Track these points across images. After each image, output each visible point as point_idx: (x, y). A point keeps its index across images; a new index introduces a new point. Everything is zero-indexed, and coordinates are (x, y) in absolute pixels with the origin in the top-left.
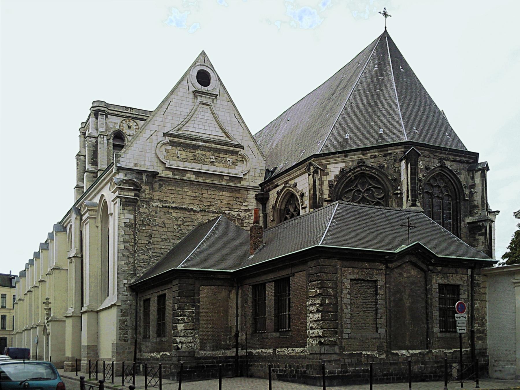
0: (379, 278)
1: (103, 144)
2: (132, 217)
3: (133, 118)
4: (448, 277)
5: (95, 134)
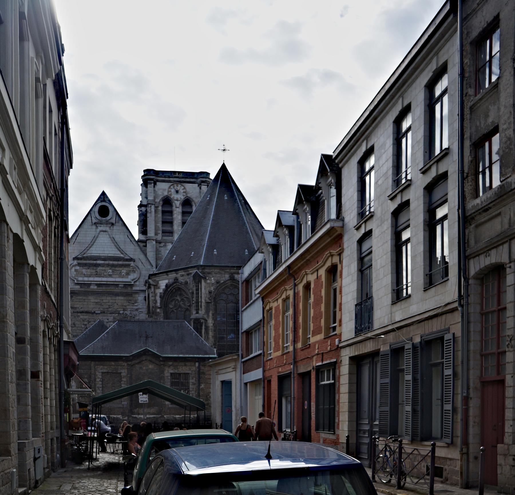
4: (178, 369)
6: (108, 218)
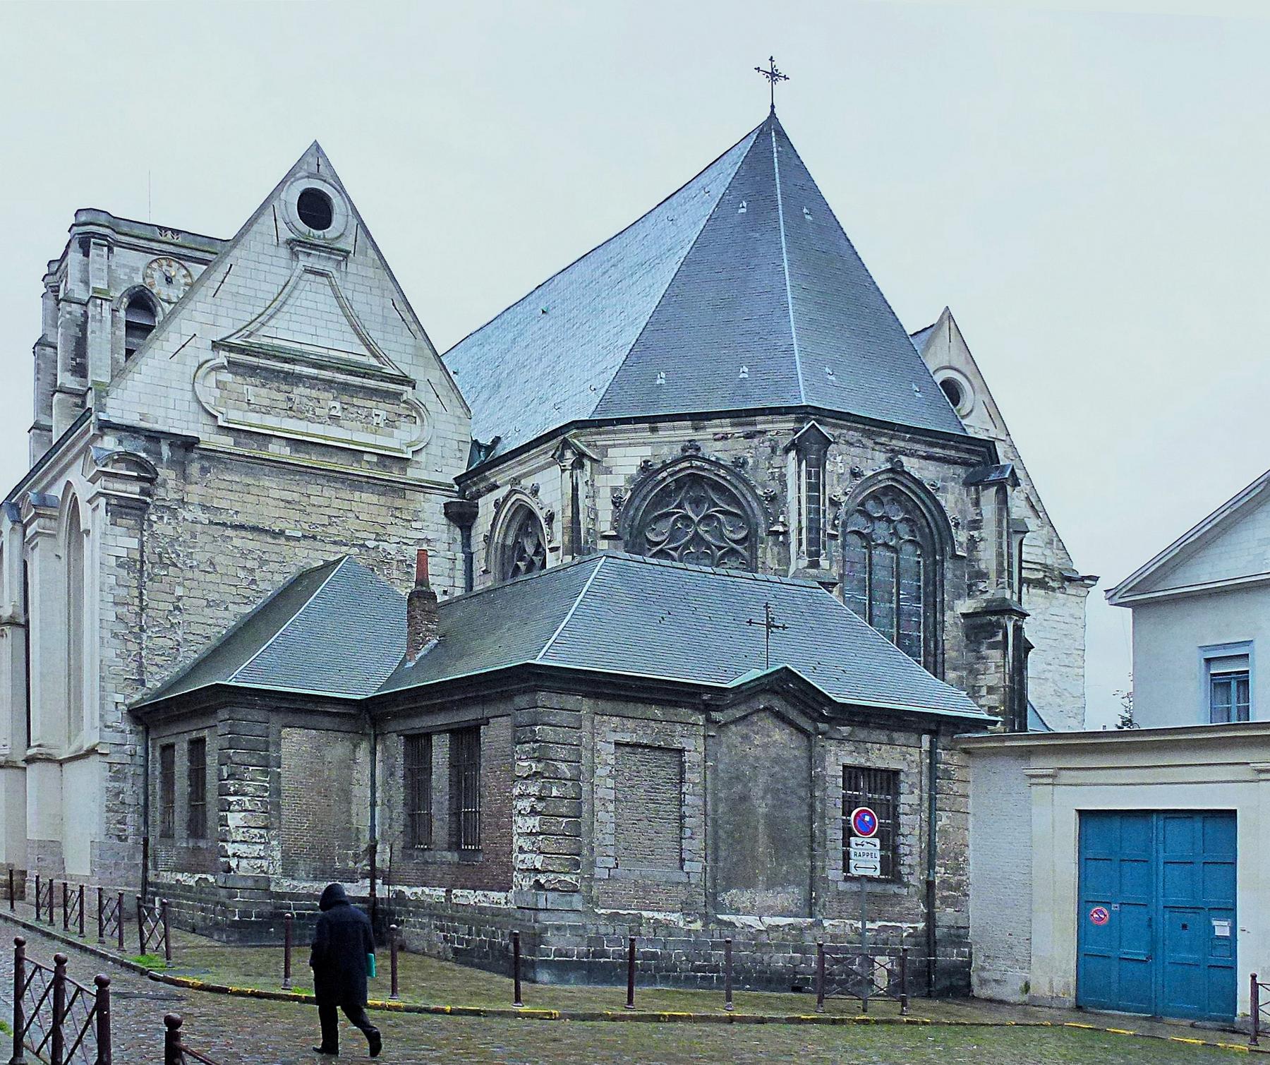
0: (688, 744)
1: (101, 321)
2: (134, 543)
3: (179, 257)
5: (81, 293)
6: (331, 232)
